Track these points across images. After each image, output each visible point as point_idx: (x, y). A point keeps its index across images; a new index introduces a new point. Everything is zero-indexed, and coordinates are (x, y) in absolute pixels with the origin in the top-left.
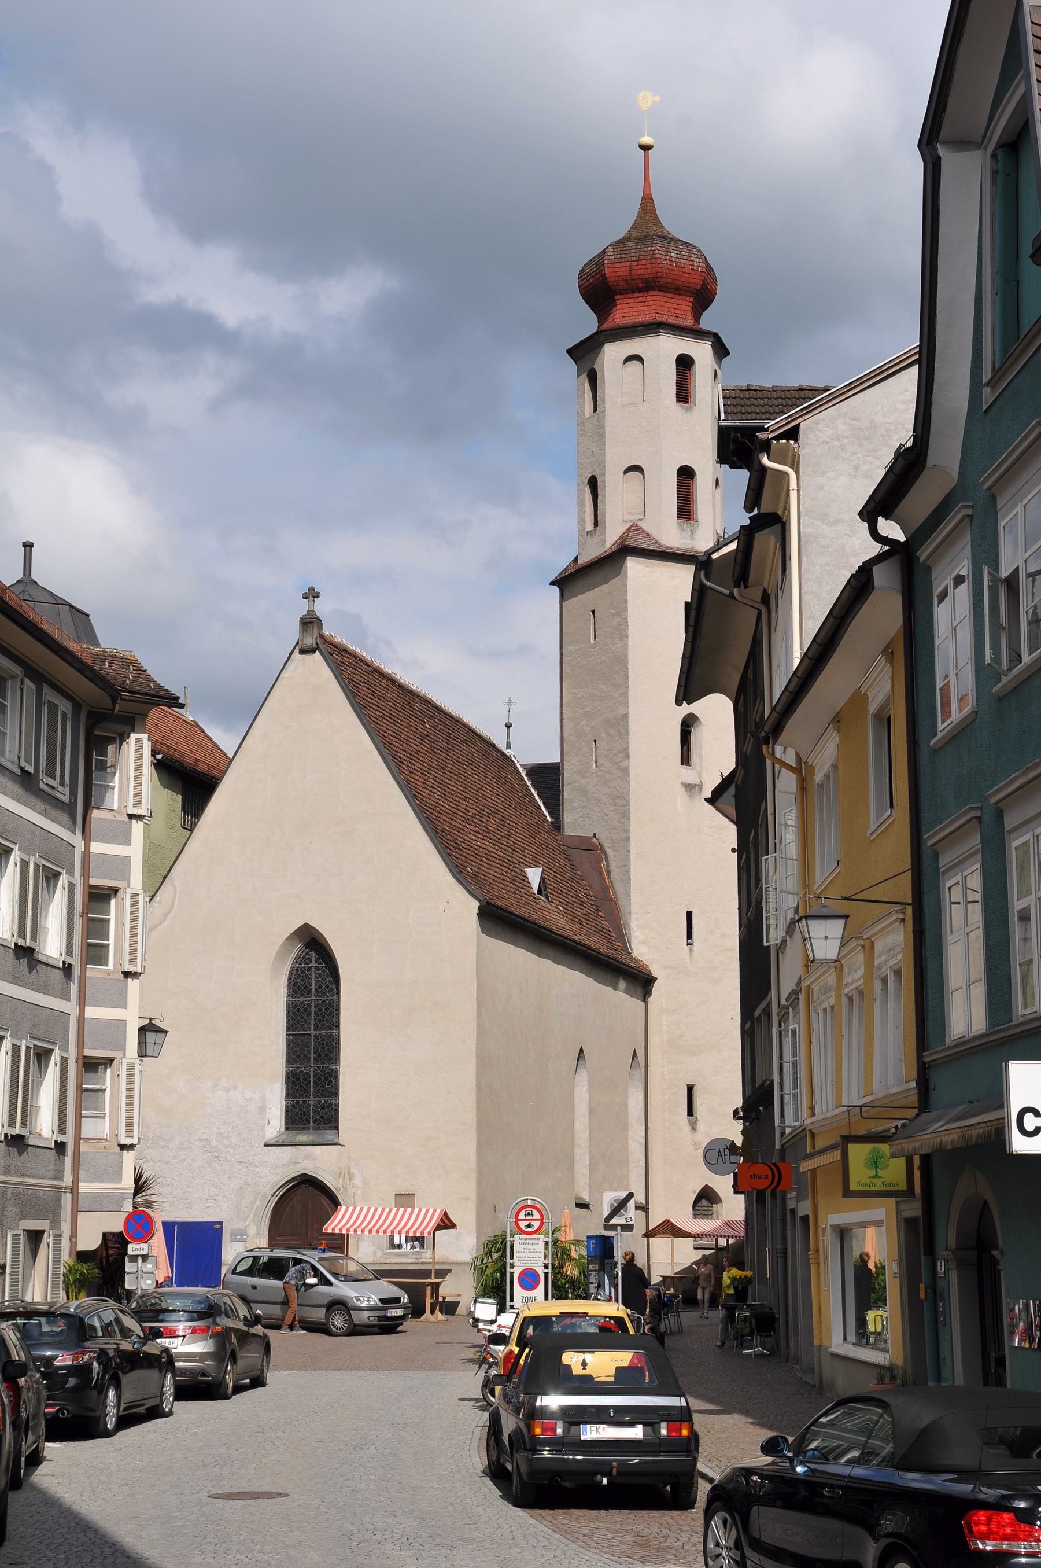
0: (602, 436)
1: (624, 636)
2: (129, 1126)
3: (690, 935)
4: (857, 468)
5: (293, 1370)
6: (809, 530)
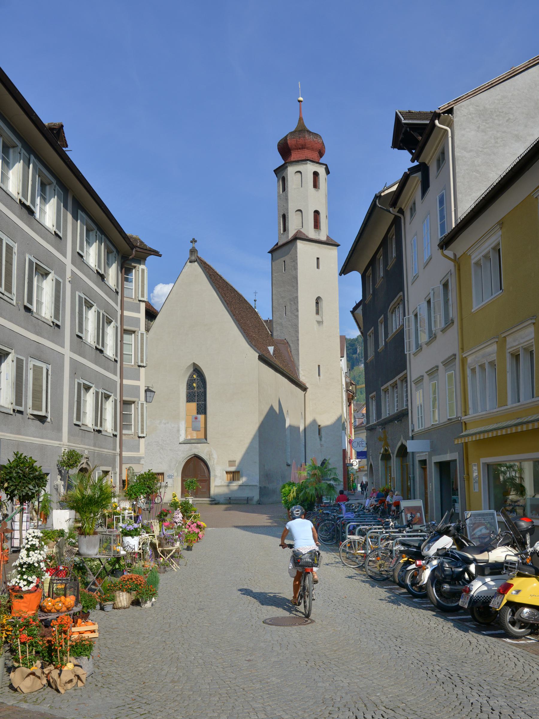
0: (287, 199)
1: (296, 269)
2: (142, 429)
3: (319, 375)
4: (479, 127)
5: (212, 527)
6: (458, 154)
